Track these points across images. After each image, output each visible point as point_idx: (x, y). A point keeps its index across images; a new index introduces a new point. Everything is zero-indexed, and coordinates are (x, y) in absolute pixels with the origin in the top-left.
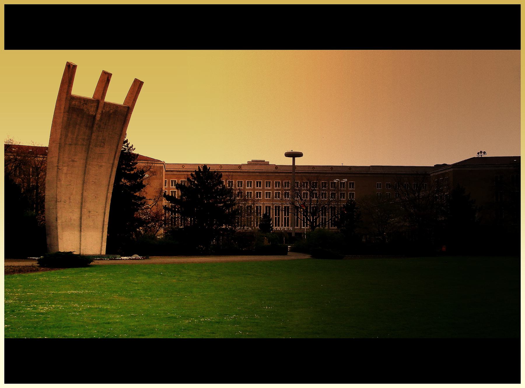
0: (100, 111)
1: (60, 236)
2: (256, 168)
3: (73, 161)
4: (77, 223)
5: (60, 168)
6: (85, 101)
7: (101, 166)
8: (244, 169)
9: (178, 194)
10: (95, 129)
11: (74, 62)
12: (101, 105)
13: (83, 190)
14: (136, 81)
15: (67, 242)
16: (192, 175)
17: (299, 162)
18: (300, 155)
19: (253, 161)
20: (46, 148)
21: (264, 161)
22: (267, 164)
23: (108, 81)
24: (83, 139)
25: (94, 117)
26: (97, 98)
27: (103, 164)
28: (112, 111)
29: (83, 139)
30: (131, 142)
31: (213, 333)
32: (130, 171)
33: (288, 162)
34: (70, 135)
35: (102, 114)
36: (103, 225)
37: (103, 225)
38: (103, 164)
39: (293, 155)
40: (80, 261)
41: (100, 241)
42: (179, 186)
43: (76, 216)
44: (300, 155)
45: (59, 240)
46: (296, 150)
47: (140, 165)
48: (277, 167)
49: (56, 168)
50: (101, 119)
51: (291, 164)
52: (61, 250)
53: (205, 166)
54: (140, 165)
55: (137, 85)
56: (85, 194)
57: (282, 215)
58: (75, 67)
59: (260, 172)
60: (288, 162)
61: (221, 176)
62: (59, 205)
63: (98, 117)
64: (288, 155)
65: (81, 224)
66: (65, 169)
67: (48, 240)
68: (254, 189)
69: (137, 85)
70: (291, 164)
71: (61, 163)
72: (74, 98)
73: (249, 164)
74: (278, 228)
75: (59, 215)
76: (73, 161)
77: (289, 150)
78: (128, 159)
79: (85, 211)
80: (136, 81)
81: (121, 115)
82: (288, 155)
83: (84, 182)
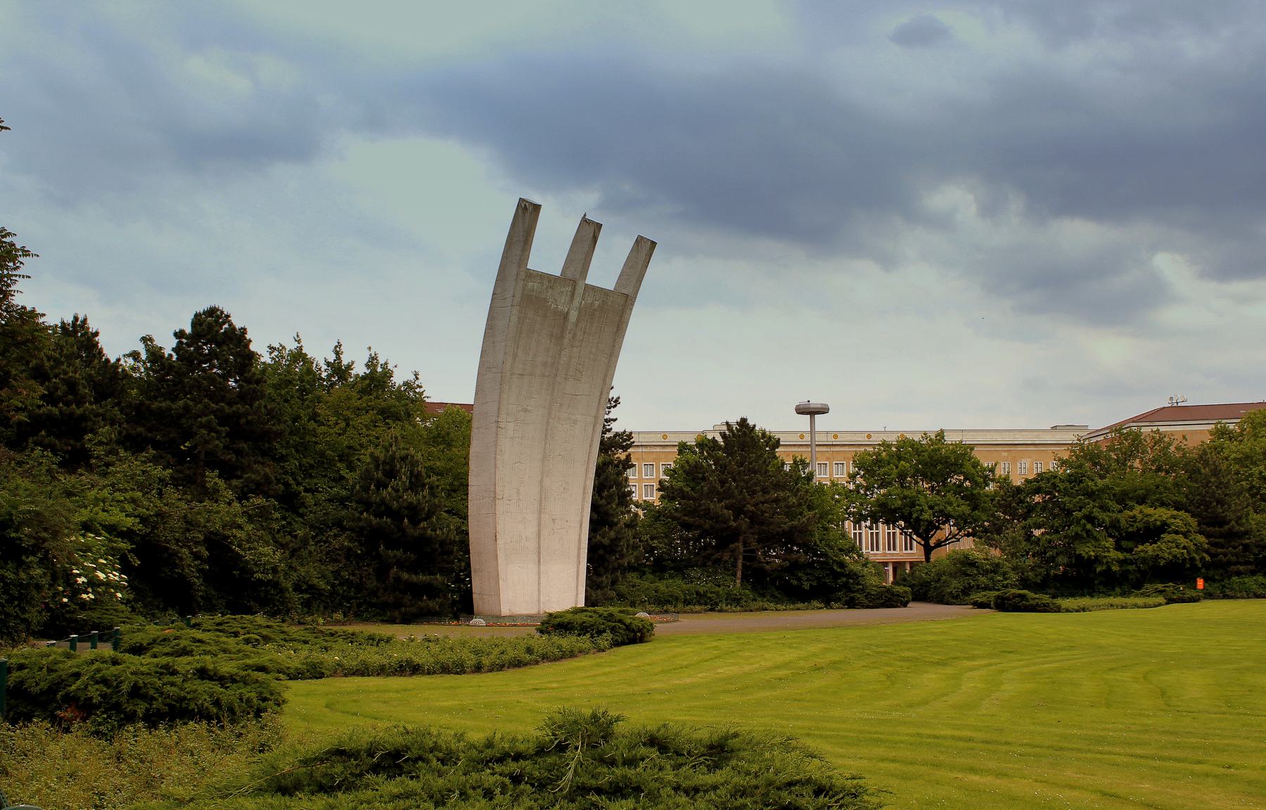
3: (526, 410)
5: (502, 425)
7: (575, 422)
10: (566, 341)
11: (536, 199)
12: (580, 290)
18: (823, 410)
24: (545, 364)
25: (566, 316)
26: (569, 275)
27: (579, 417)
29: (545, 364)
31: (854, 778)
34: (520, 353)
35: (580, 310)
36: (579, 549)
37: (579, 549)
38: (579, 417)
41: (573, 585)
43: (531, 530)
44: (823, 410)
45: (501, 583)
46: (816, 401)
49: (494, 425)
50: (578, 320)
52: (505, 611)
58: (537, 208)
62: (500, 506)
63: (573, 316)
65: (539, 547)
67: (815, 603)
69: (144, 340)
71: (503, 416)
72: (531, 275)
75: (499, 528)
76: (526, 410)
77: (801, 400)
82: (801, 411)
83: (544, 458)
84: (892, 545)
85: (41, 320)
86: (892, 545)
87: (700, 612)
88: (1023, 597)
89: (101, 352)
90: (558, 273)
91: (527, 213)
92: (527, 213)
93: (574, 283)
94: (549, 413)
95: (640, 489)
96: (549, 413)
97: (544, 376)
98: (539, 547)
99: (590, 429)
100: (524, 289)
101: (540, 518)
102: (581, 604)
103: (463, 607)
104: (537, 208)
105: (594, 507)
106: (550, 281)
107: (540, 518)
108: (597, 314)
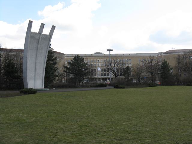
0: (41, 37)
1: (28, 82)
2: (98, 55)
3: (32, 55)
4: (34, 77)
6: (36, 33)
8: (93, 55)
9: (68, 66)
11: (32, 21)
12: (41, 35)
13: (36, 65)
14: (42, 24)
15: (31, 84)
16: (73, 59)
17: (112, 52)
18: (112, 50)
19: (159, 53)
20: (18, 52)
21: (100, 53)
22: (101, 53)
23: (44, 27)
25: (39, 40)
28: (45, 37)
30: (52, 48)
32: (52, 58)
33: (108, 52)
39: (110, 50)
40: (33, 92)
41: (41, 83)
42: (69, 63)
43: (33, 75)
46: (110, 48)
47: (56, 55)
48: (104, 54)
50: (41, 40)
51: (109, 53)
52: (29, 88)
53: (78, 56)
54: (56, 55)
55: (53, 28)
56: (36, 67)
57: (103, 72)
58: (32, 22)
59: (98, 56)
60: (108, 52)
61: (83, 59)
63: (40, 39)
64: (108, 50)
66: (29, 58)
68: (97, 63)
69: (53, 28)
70: (109, 53)
73: (95, 53)
74: (105, 77)
77: (108, 49)
78: (51, 53)
79: (36, 73)
80: (42, 24)
81: (49, 37)
82: (108, 50)
84: (108, 75)
86: (108, 75)
88: (118, 86)
90: (38, 32)
91: (31, 23)
92: (31, 23)
93: (40, 34)
101: (35, 73)
102: (43, 87)
103: (24, 88)
104: (32, 22)
105: (46, 71)
107: (35, 73)
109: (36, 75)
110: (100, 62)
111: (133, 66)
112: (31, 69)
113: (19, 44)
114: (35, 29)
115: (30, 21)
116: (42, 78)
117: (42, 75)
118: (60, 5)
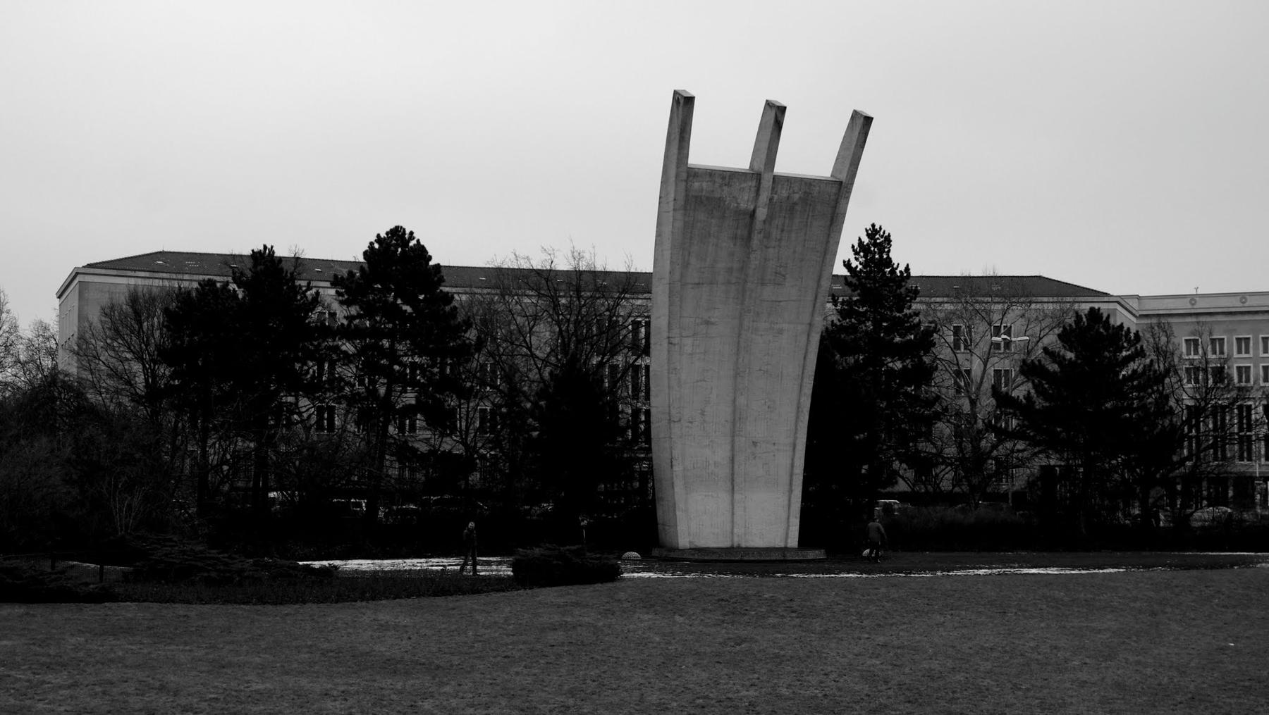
0: (764, 197)
3: (708, 323)
4: (724, 472)
5: (676, 341)
6: (728, 177)
7: (780, 332)
12: (767, 183)
20: (631, 283)
23: (778, 125)
24: (730, 270)
27: (785, 326)
34: (693, 260)
36: (791, 475)
37: (791, 475)
38: (785, 326)
43: (722, 454)
50: (769, 219)
52: (684, 542)
63: (762, 213)
65: (733, 474)
75: (676, 453)
76: (708, 323)
81: (828, 198)
85: (54, 328)
87: (104, 595)
89: (241, 256)
94: (741, 325)
95: (1256, 343)
96: (741, 325)
97: (729, 282)
98: (733, 474)
99: (804, 338)
100: (687, 190)
102: (793, 542)
106: (723, 178)
108: (798, 208)
109: (740, 458)
110: (1256, 354)
111: (83, 349)
112: (703, 413)
113: (620, 235)
114: (722, 145)
115: (676, 93)
116: (784, 478)
117: (783, 460)
118: (383, 235)
